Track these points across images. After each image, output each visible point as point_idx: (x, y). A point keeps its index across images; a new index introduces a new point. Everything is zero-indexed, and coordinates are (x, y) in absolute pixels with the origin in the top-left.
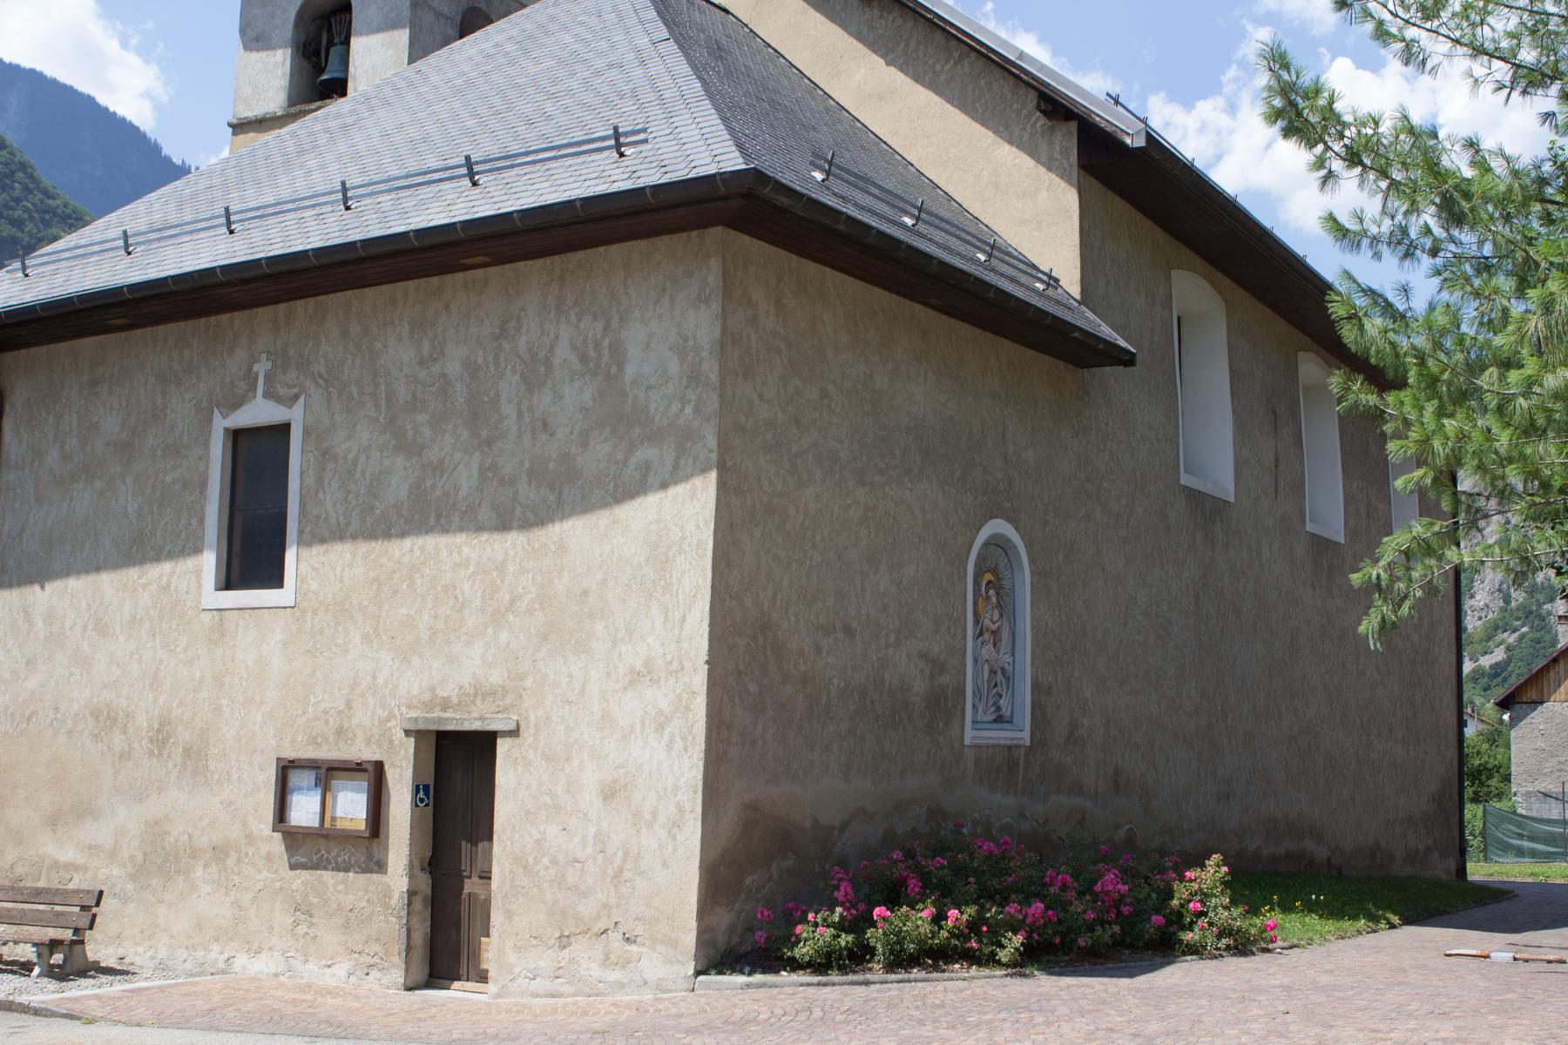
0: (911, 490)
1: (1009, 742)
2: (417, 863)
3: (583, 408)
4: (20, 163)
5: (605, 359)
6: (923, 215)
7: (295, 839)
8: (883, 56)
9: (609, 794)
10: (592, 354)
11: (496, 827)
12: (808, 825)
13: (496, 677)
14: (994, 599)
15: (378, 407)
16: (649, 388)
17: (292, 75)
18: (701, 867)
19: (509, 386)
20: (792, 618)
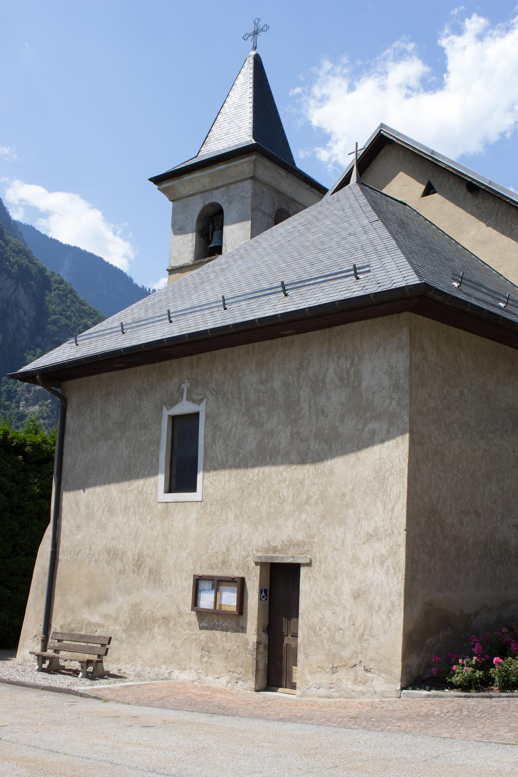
0: (507, 441)
2: (261, 628)
4: (70, 289)
5: (352, 379)
6: (509, 301)
8: (484, 222)
9: (356, 596)
11: (300, 611)
13: (300, 537)
15: (241, 404)
16: (374, 393)
17: (196, 245)
18: (403, 634)
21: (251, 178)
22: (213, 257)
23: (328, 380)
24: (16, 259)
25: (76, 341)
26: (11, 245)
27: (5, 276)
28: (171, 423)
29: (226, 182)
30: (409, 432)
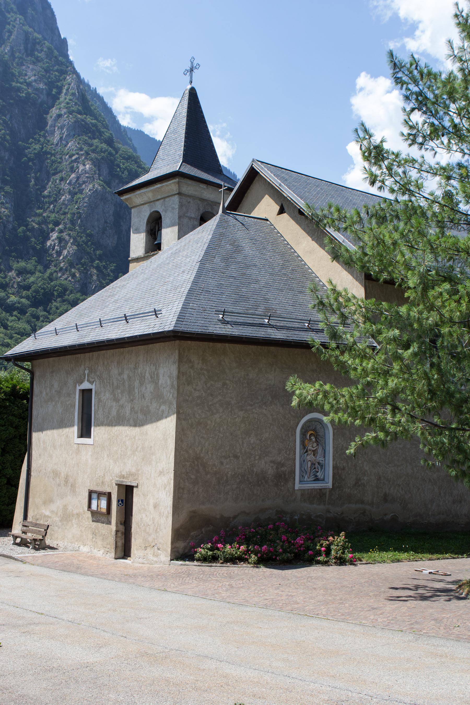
0: (266, 409)
1: (320, 488)
2: (119, 522)
3: (151, 392)
5: (155, 378)
6: (271, 318)
7: (94, 513)
8: (311, 237)
9: (155, 507)
10: (153, 376)
11: (133, 514)
12: (218, 517)
13: (134, 470)
14: (314, 440)
15: (110, 387)
16: (164, 388)
17: (146, 242)
18: (172, 529)
19: (137, 384)
20: (210, 455)
21: (178, 194)
22: (156, 252)
23: (146, 377)
24: (126, 165)
25: (35, 337)
26: (120, 152)
27: (117, 181)
28: (81, 394)
29: (163, 196)
30: (178, 413)
